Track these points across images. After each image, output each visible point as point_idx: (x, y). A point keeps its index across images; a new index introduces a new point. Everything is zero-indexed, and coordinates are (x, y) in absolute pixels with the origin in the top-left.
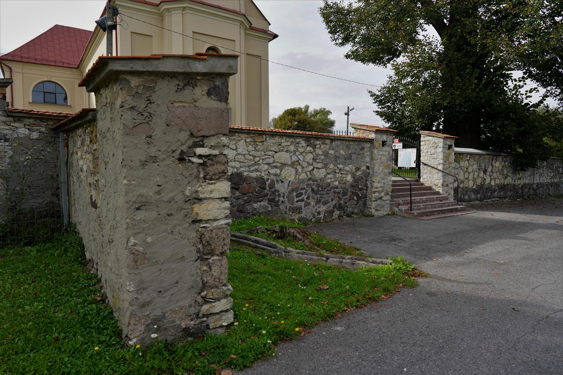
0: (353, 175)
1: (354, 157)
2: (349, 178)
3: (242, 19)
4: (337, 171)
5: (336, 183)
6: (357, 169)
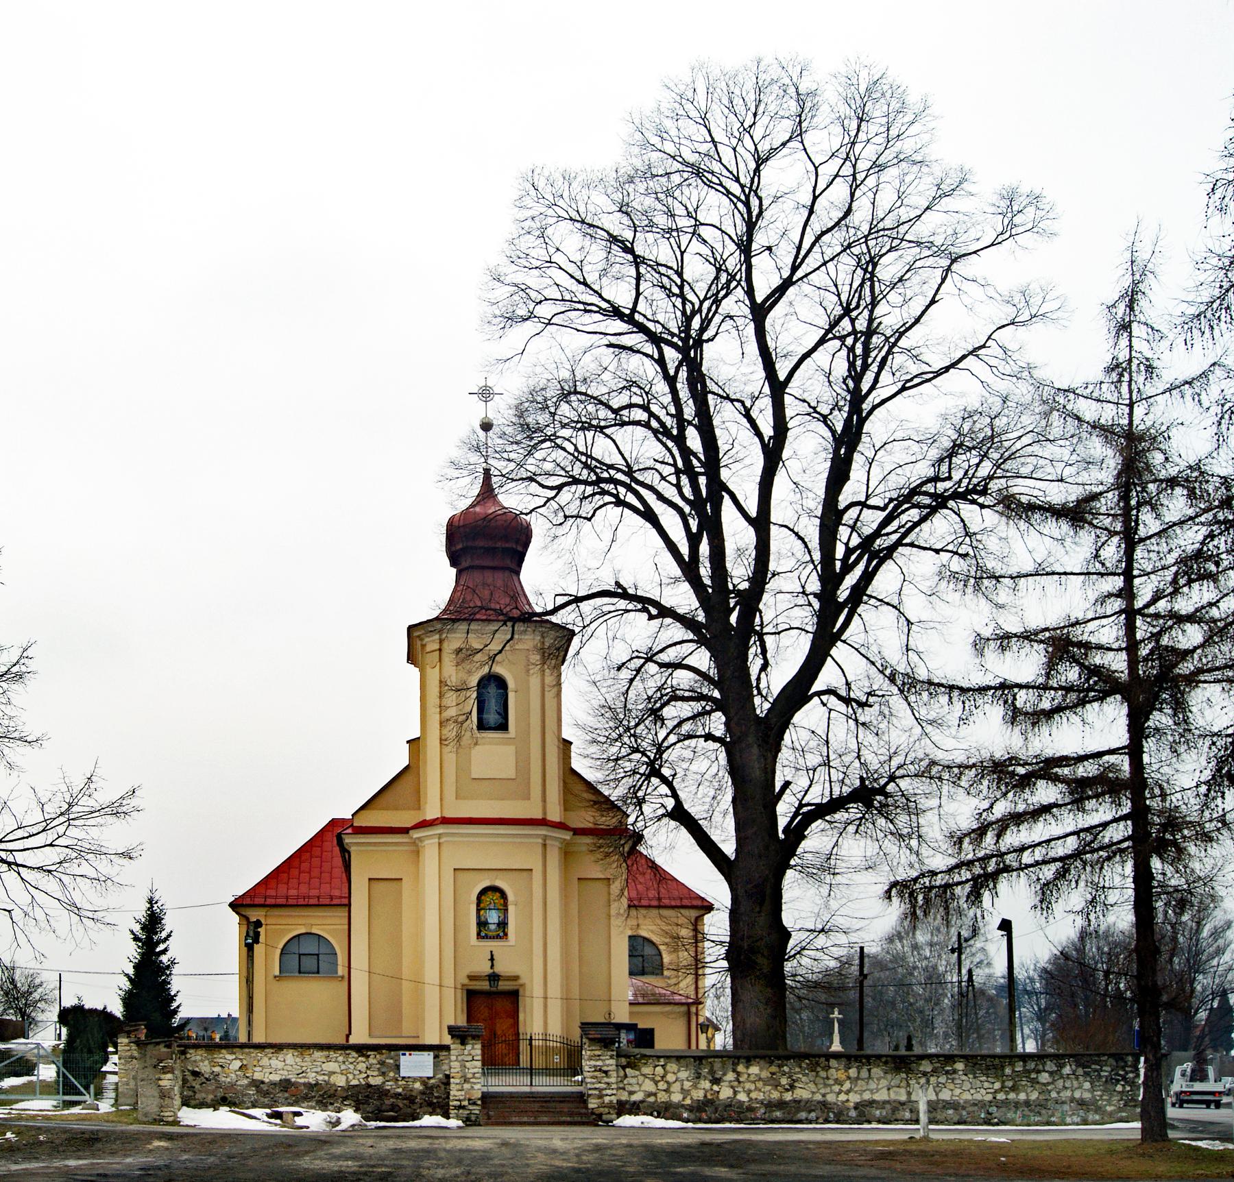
3: (544, 832)
5: (400, 1090)
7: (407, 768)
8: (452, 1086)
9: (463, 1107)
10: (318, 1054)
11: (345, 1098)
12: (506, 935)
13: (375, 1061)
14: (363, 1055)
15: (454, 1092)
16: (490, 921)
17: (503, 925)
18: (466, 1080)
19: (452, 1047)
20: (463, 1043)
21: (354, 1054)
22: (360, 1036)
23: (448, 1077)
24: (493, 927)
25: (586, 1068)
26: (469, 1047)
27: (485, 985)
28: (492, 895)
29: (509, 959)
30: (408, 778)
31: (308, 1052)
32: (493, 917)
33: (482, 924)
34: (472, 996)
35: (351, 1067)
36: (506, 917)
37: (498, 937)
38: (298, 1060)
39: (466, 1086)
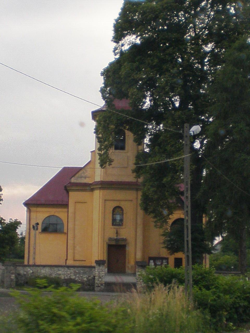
0: (87, 278)
1: (87, 273)
2: (85, 279)
4: (80, 277)
6: (89, 277)
7: (90, 161)
8: (96, 280)
9: (99, 286)
10: (56, 269)
11: (189, 58)
12: (122, 224)
13: (72, 271)
14: (69, 269)
15: (96, 282)
16: (117, 219)
17: (121, 220)
18: (100, 278)
19: (96, 267)
20: (99, 266)
21: (66, 269)
22: (70, 262)
23: (94, 277)
24: (118, 221)
25: (137, 275)
26: (101, 267)
27: (113, 243)
28: (117, 210)
29: (126, 233)
30: (91, 166)
31: (53, 268)
32: (118, 217)
33: (114, 220)
34: (110, 247)
35: (66, 273)
36: (123, 217)
37: (119, 225)
38: (50, 270)
39: (100, 280)
